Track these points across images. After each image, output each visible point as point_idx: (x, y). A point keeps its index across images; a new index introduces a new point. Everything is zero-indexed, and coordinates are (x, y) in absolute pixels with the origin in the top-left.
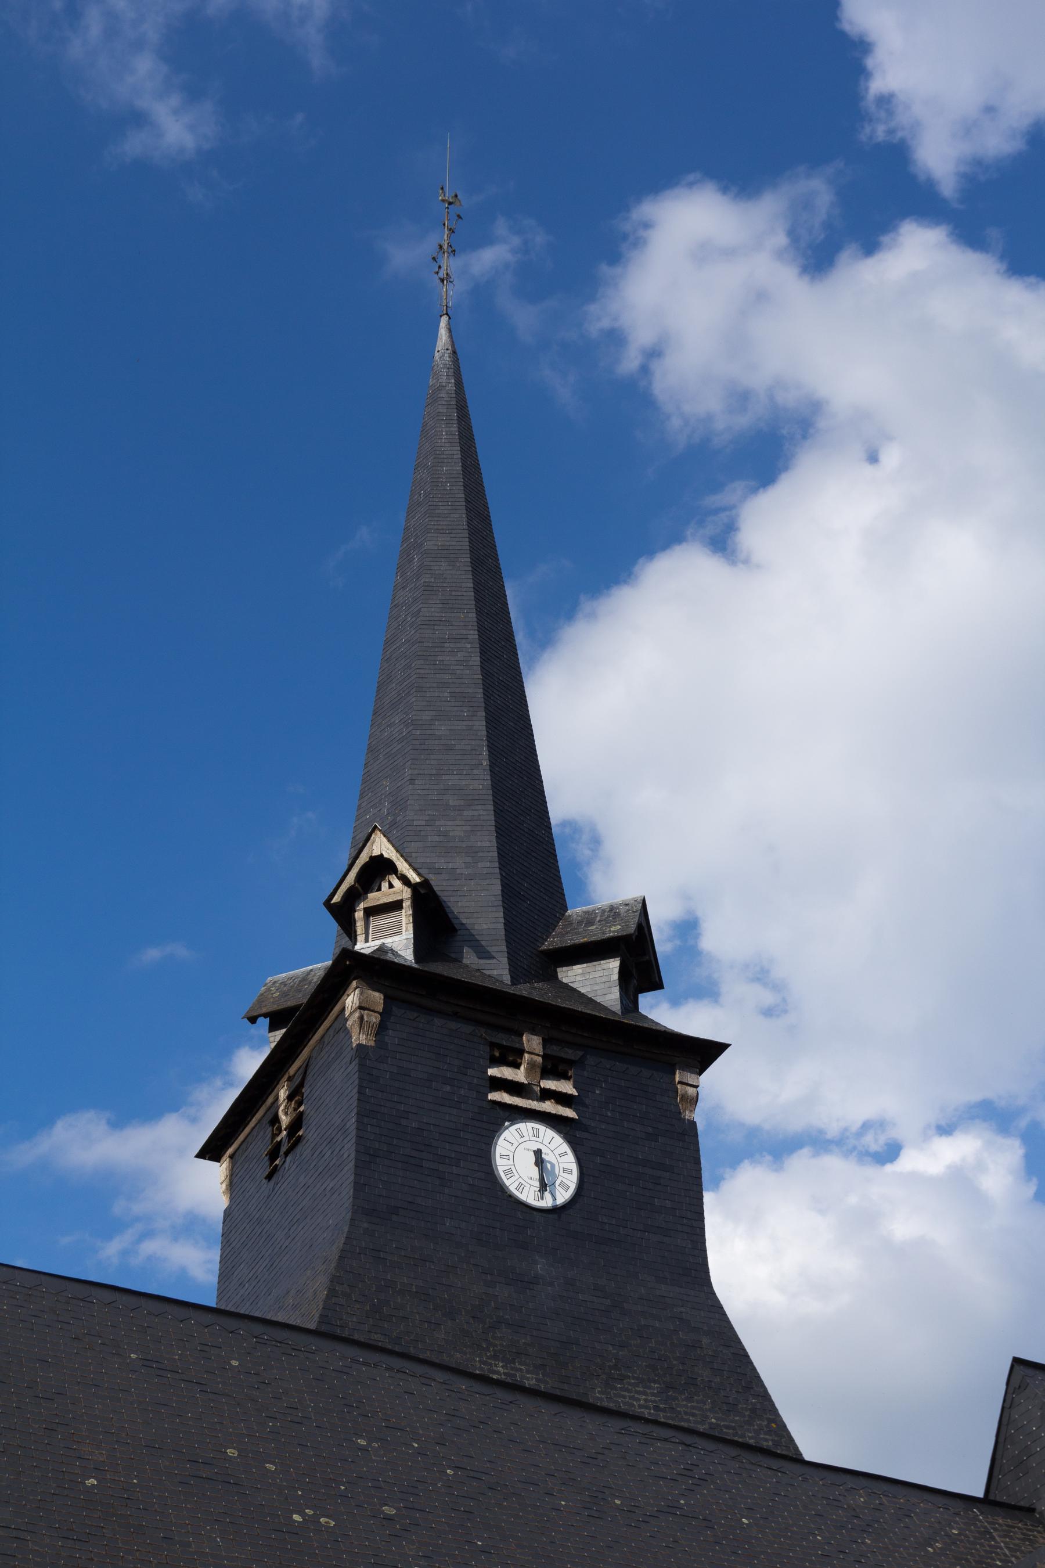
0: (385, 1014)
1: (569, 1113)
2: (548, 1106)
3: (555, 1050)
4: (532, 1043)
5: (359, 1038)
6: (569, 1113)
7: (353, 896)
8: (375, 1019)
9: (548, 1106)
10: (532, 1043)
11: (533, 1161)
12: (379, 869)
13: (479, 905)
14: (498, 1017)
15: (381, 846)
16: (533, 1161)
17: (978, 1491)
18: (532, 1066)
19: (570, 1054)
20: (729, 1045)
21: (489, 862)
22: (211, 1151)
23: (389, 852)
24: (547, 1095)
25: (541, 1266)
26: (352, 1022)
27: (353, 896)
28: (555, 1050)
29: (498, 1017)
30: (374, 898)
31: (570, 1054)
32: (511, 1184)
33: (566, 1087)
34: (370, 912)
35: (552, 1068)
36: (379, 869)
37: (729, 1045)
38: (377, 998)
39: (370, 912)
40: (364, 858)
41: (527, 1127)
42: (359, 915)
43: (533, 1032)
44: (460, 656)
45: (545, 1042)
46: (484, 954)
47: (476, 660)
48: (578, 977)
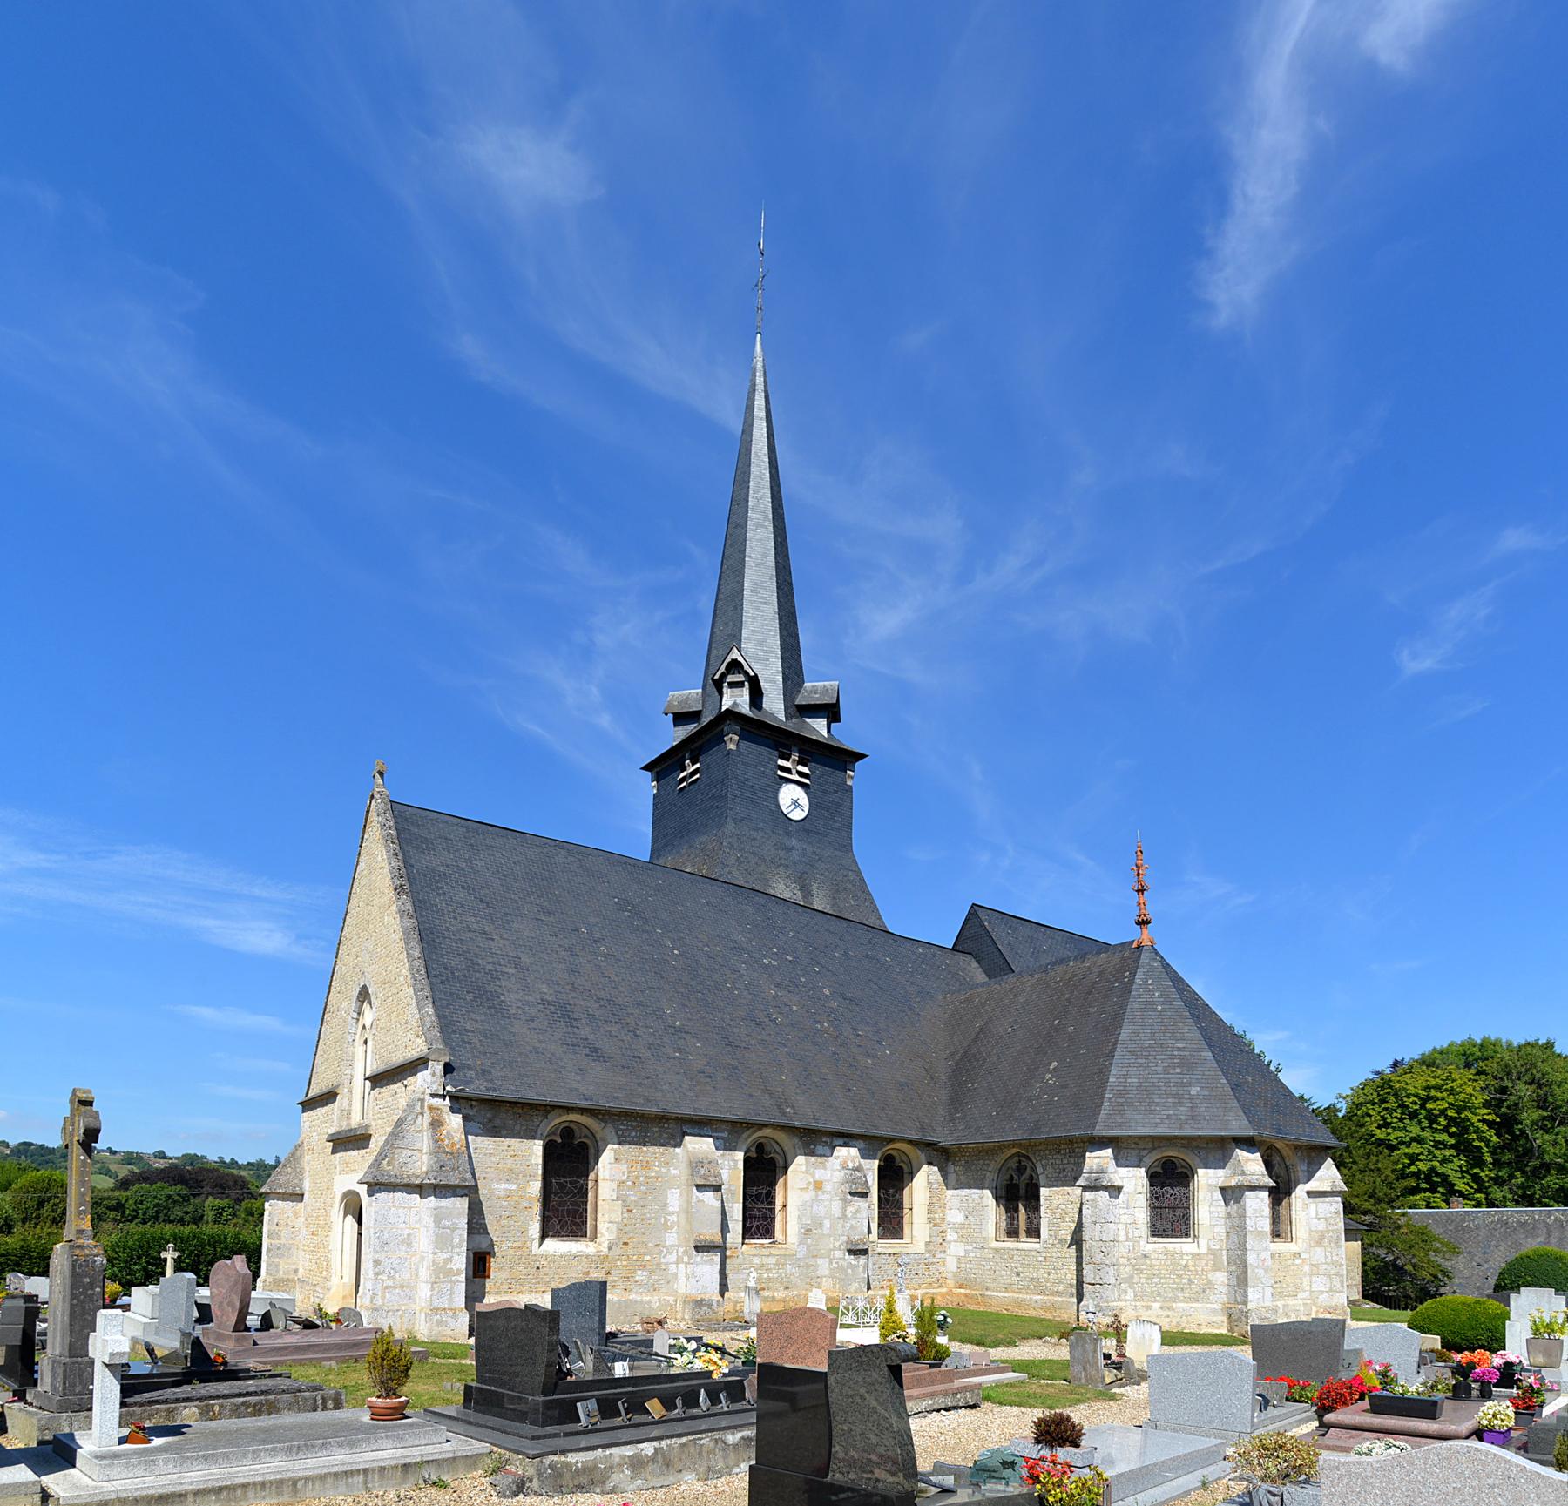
2: (796, 777)
20: (860, 756)
25: (794, 842)
35: (801, 762)
37: (860, 756)
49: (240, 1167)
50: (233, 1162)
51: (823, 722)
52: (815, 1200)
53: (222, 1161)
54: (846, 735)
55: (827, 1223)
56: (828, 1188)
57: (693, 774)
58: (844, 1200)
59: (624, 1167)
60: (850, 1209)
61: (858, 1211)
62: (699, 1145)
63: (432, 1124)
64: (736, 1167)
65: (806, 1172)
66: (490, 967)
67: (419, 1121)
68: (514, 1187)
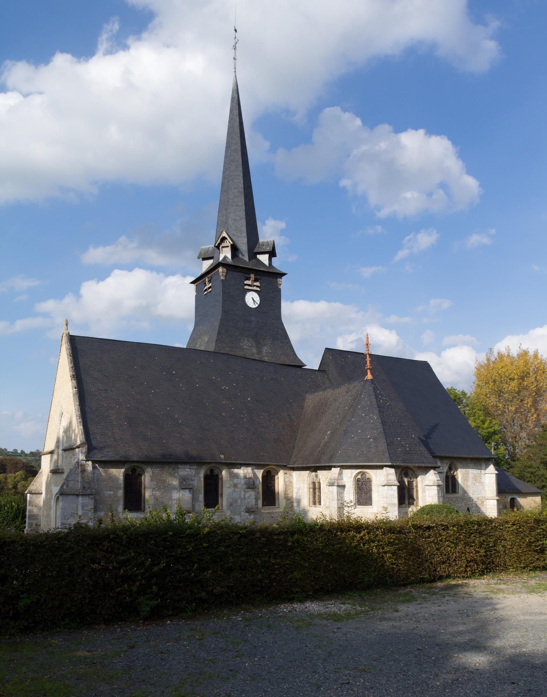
0: (226, 273)
1: (258, 289)
2: (255, 288)
3: (257, 277)
4: (252, 276)
5: (222, 278)
6: (258, 289)
7: (219, 244)
8: (225, 274)
9: (255, 288)
10: (252, 276)
11: (252, 299)
12: (224, 239)
13: (243, 246)
14: (246, 272)
15: (224, 234)
16: (252, 299)
17: (317, 368)
18: (252, 280)
19: (259, 277)
20: (284, 274)
21: (245, 234)
22: (193, 283)
23: (226, 236)
24: (254, 286)
25: (253, 319)
26: (221, 274)
27: (219, 244)
28: (257, 277)
29: (246, 272)
30: (223, 245)
31: (259, 277)
32: (248, 304)
33: (258, 284)
34: (222, 247)
35: (256, 280)
36: (224, 239)
37: (284, 274)
38: (225, 270)
39: (222, 247)
40: (221, 237)
41: (251, 293)
42: (221, 248)
43: (253, 273)
44: (239, 180)
45: (255, 275)
46: (243, 255)
47: (242, 181)
48: (260, 257)
49: (26, 455)
50: (23, 452)
51: (267, 256)
52: (234, 491)
53: (16, 451)
54: (278, 264)
55: (239, 501)
56: (239, 486)
57: (209, 288)
58: (244, 491)
59: (155, 483)
60: (247, 495)
61: (250, 496)
62: (186, 471)
63: (81, 472)
64: (200, 480)
65: (230, 480)
66: (105, 405)
67: (77, 470)
68: (112, 493)
